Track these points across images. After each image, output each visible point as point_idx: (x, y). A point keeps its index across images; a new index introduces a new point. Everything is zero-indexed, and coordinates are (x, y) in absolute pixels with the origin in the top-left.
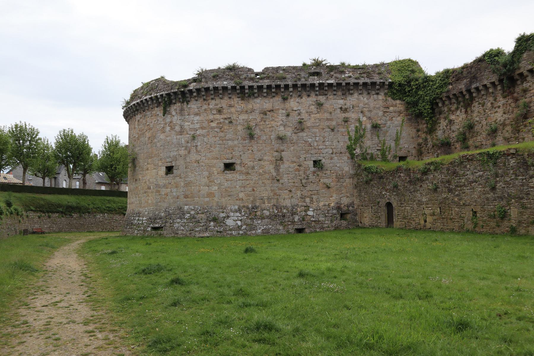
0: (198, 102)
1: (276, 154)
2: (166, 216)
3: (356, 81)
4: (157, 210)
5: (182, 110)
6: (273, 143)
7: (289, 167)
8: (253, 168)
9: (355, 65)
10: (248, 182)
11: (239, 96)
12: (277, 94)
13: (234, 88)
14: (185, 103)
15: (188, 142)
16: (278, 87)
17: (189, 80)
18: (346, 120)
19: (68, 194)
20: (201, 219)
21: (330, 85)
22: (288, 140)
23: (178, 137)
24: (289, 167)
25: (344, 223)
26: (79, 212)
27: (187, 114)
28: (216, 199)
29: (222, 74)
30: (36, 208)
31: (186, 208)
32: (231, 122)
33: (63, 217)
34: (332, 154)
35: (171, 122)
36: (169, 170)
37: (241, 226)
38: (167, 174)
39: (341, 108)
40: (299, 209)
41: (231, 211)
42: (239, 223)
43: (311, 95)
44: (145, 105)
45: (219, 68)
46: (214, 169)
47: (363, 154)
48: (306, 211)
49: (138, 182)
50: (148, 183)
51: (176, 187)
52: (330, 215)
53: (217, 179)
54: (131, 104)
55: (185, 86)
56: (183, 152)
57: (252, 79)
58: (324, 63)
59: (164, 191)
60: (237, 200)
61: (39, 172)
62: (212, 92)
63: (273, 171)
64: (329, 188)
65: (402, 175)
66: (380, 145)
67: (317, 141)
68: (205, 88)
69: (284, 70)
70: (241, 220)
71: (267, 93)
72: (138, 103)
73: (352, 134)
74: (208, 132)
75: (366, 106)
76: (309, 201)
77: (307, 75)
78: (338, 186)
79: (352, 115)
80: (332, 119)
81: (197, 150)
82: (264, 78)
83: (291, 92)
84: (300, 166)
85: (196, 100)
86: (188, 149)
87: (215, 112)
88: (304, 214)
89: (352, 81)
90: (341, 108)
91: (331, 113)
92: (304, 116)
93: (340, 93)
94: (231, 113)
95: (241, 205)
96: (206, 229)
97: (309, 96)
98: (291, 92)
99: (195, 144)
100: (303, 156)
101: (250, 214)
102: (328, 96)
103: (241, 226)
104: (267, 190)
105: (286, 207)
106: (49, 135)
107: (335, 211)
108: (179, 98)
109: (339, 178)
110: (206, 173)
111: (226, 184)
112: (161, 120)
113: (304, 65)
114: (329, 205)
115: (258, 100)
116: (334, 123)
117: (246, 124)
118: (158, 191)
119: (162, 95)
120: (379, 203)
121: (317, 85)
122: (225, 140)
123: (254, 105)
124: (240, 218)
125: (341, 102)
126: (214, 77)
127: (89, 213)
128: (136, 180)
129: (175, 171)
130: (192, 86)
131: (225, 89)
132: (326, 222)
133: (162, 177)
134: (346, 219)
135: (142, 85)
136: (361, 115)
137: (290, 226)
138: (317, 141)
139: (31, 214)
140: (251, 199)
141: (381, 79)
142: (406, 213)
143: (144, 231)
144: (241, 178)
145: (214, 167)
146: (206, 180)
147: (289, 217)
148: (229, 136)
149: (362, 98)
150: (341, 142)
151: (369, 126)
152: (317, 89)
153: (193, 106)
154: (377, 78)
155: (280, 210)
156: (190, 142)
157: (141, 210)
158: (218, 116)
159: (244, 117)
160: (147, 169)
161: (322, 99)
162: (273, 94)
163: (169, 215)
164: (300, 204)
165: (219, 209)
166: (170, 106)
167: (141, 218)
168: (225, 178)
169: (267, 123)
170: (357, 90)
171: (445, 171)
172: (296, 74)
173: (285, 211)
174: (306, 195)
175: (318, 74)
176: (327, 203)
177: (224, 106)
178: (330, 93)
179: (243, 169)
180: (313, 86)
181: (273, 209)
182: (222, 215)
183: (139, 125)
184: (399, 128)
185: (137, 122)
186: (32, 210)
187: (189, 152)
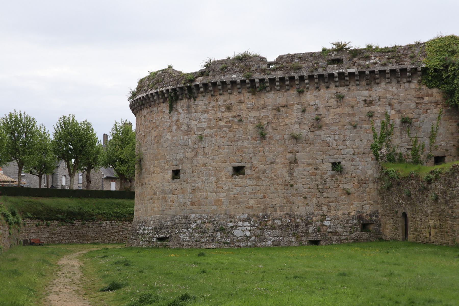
0: (206, 98)
1: (289, 156)
2: (172, 226)
3: (382, 68)
4: (162, 218)
5: (189, 107)
6: (287, 143)
7: (304, 170)
8: (264, 172)
9: (383, 47)
10: (258, 188)
11: (249, 90)
12: (292, 86)
13: (243, 82)
14: (192, 99)
15: (195, 143)
16: (292, 79)
17: (196, 73)
18: (371, 115)
19: (69, 197)
20: (208, 229)
21: (352, 75)
22: (304, 139)
23: (185, 137)
24: (304, 170)
25: (365, 235)
26: (82, 219)
27: (194, 111)
28: (224, 207)
29: (231, 65)
30: (34, 214)
31: (193, 216)
32: (240, 121)
33: (63, 225)
34: (353, 154)
35: (177, 120)
36: (176, 174)
37: (250, 237)
38: (173, 178)
39: (365, 101)
40: (314, 219)
41: (240, 220)
42: (248, 234)
43: (331, 86)
44: (151, 99)
45: (229, 58)
46: (223, 173)
47: (390, 154)
48: (322, 221)
49: (144, 186)
50: (154, 188)
51: (183, 193)
52: (350, 225)
53: (225, 184)
54: (137, 97)
55: (192, 81)
56: (189, 154)
57: (263, 71)
58: (347, 47)
59: (170, 197)
60: (246, 208)
61: (35, 168)
62: (220, 87)
63: (286, 175)
64: (349, 194)
65: (414, 182)
66: (411, 143)
67: (336, 140)
68: (212, 83)
69: (300, 58)
70: (250, 231)
71: (280, 86)
72: (143, 97)
73: (378, 131)
74: (216, 131)
75: (396, 97)
76: (326, 210)
77: (326, 64)
78: (360, 192)
79: (378, 109)
80: (355, 113)
81: (204, 153)
82: (277, 68)
83: (307, 84)
84: (316, 169)
85: (204, 96)
86: (195, 151)
87: (223, 109)
88: (319, 224)
89: (377, 68)
90: (365, 101)
91: (353, 107)
92: (322, 111)
93: (364, 83)
94: (241, 110)
95: (251, 213)
96: (213, 240)
97: (328, 87)
98: (307, 84)
99: (202, 146)
100: (320, 158)
101: (260, 223)
102: (350, 86)
103: (250, 237)
104: (279, 197)
105: (300, 216)
106: (48, 125)
107: (355, 222)
108: (186, 94)
109: (361, 183)
110: (214, 178)
111: (235, 190)
112: (167, 117)
113: (324, 50)
114: (349, 214)
115: (271, 95)
116: (356, 119)
117: (257, 122)
118: (164, 198)
119: (167, 90)
120: (397, 212)
121: (336, 75)
122: (235, 141)
123: (267, 101)
124: (249, 228)
125: (366, 93)
126: (222, 69)
127: (93, 220)
128: (142, 184)
129: (181, 175)
130: (199, 81)
131: (233, 83)
132: (345, 233)
133: (168, 181)
134: (367, 229)
135: (148, 74)
136: (388, 109)
137: (303, 238)
138: (336, 140)
139: (28, 222)
140: (262, 207)
141: (413, 64)
142: (417, 225)
143: (150, 242)
144: (251, 183)
145: (222, 171)
146: (213, 186)
147: (303, 228)
148: (238, 136)
149: (390, 88)
150: (365, 140)
151: (398, 121)
152: (337, 79)
153: (200, 103)
154: (409, 63)
155: (293, 219)
156: (197, 143)
157: (147, 218)
158: (227, 114)
159: (255, 114)
160: (154, 173)
161: (343, 90)
162: (287, 87)
163: (175, 225)
164: (316, 212)
165: (227, 218)
166: (177, 103)
167: (146, 228)
168: (233, 184)
169: (280, 120)
170: (385, 78)
171: (443, 181)
172: (313, 62)
173: (298, 220)
174: (323, 202)
175: (338, 61)
176: (347, 212)
177: (233, 102)
178: (352, 83)
179: (254, 173)
180: (331, 76)
181: (285, 218)
182: (230, 225)
183: (145, 122)
184: (435, 123)
185: (143, 118)
186: (29, 217)
187: (196, 155)
